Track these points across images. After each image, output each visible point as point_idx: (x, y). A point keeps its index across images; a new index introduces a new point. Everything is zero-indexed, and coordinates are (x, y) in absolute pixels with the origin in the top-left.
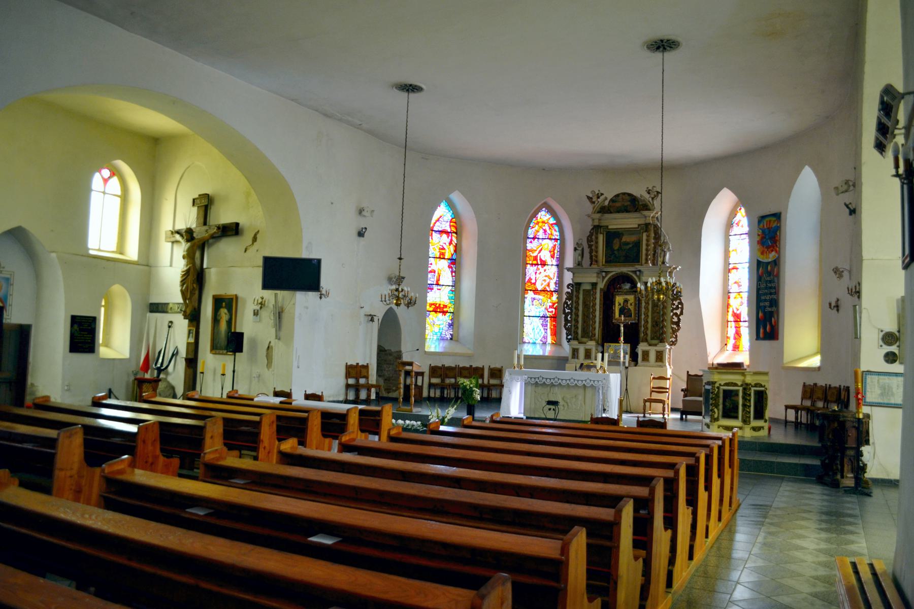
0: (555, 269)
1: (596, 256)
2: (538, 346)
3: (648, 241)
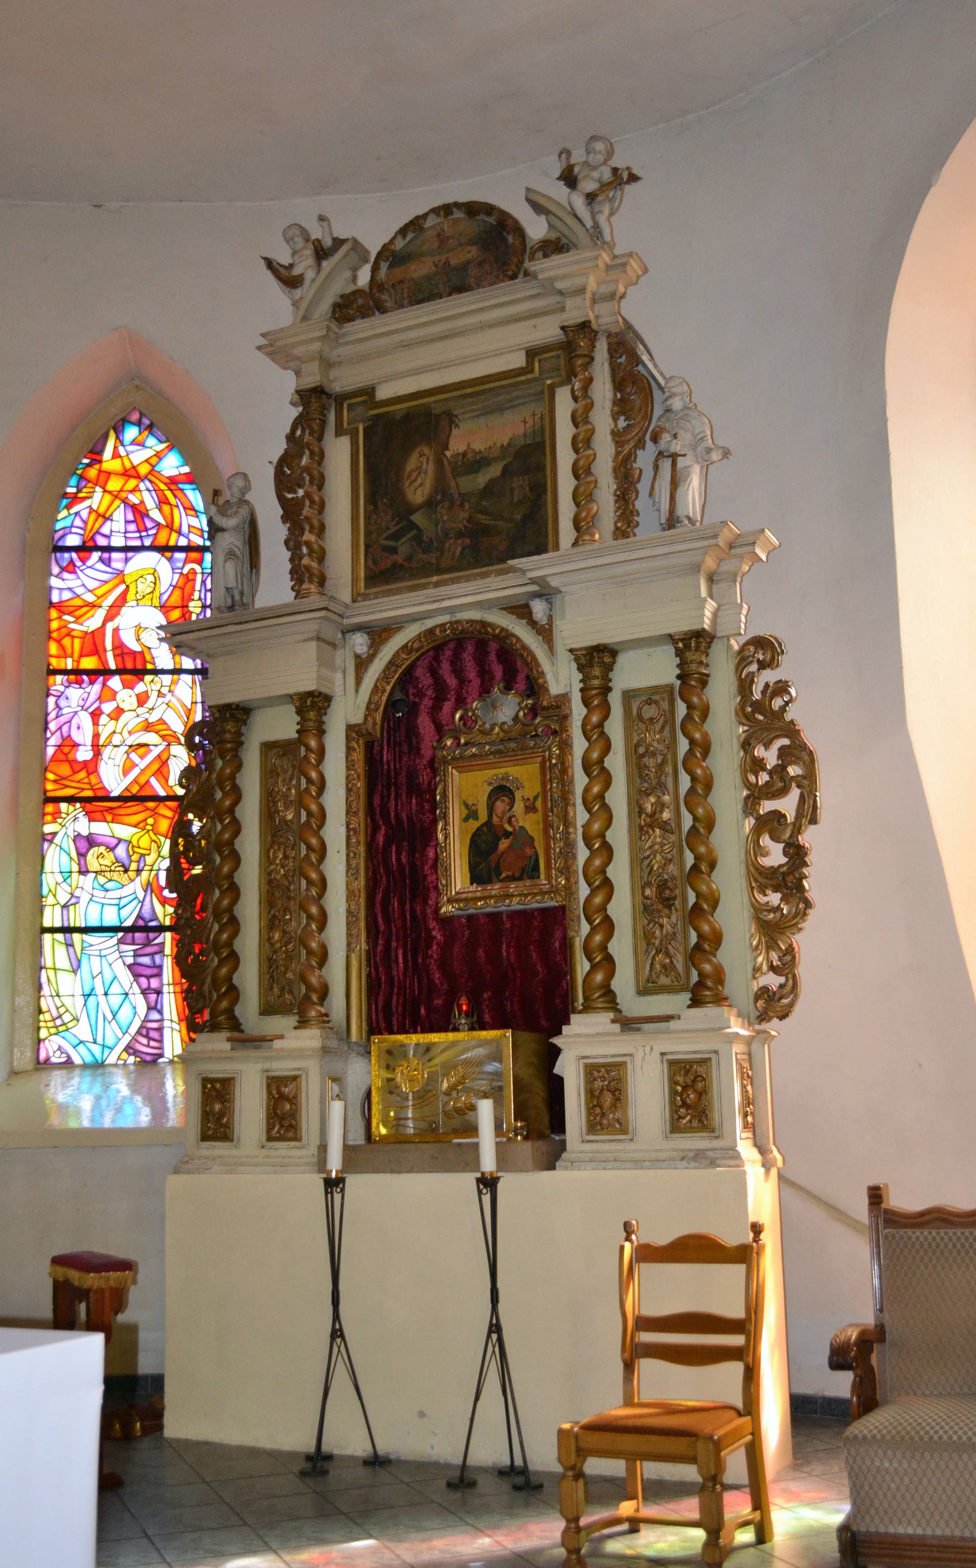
1: (321, 556)
2: (121, 1086)
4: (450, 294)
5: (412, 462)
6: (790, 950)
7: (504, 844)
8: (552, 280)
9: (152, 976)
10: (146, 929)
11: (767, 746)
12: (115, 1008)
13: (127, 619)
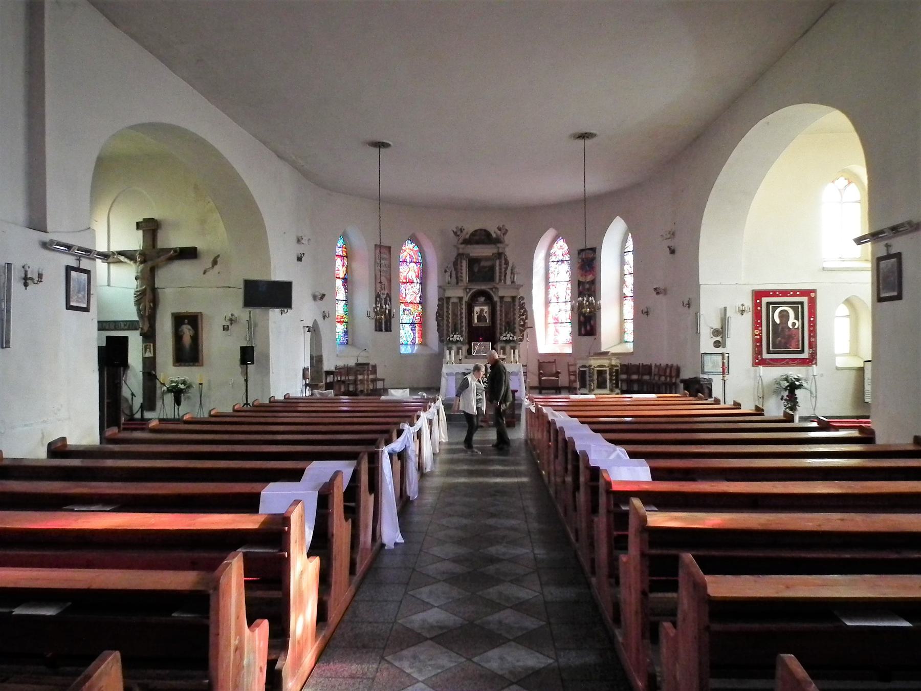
0: (418, 286)
3: (500, 265)
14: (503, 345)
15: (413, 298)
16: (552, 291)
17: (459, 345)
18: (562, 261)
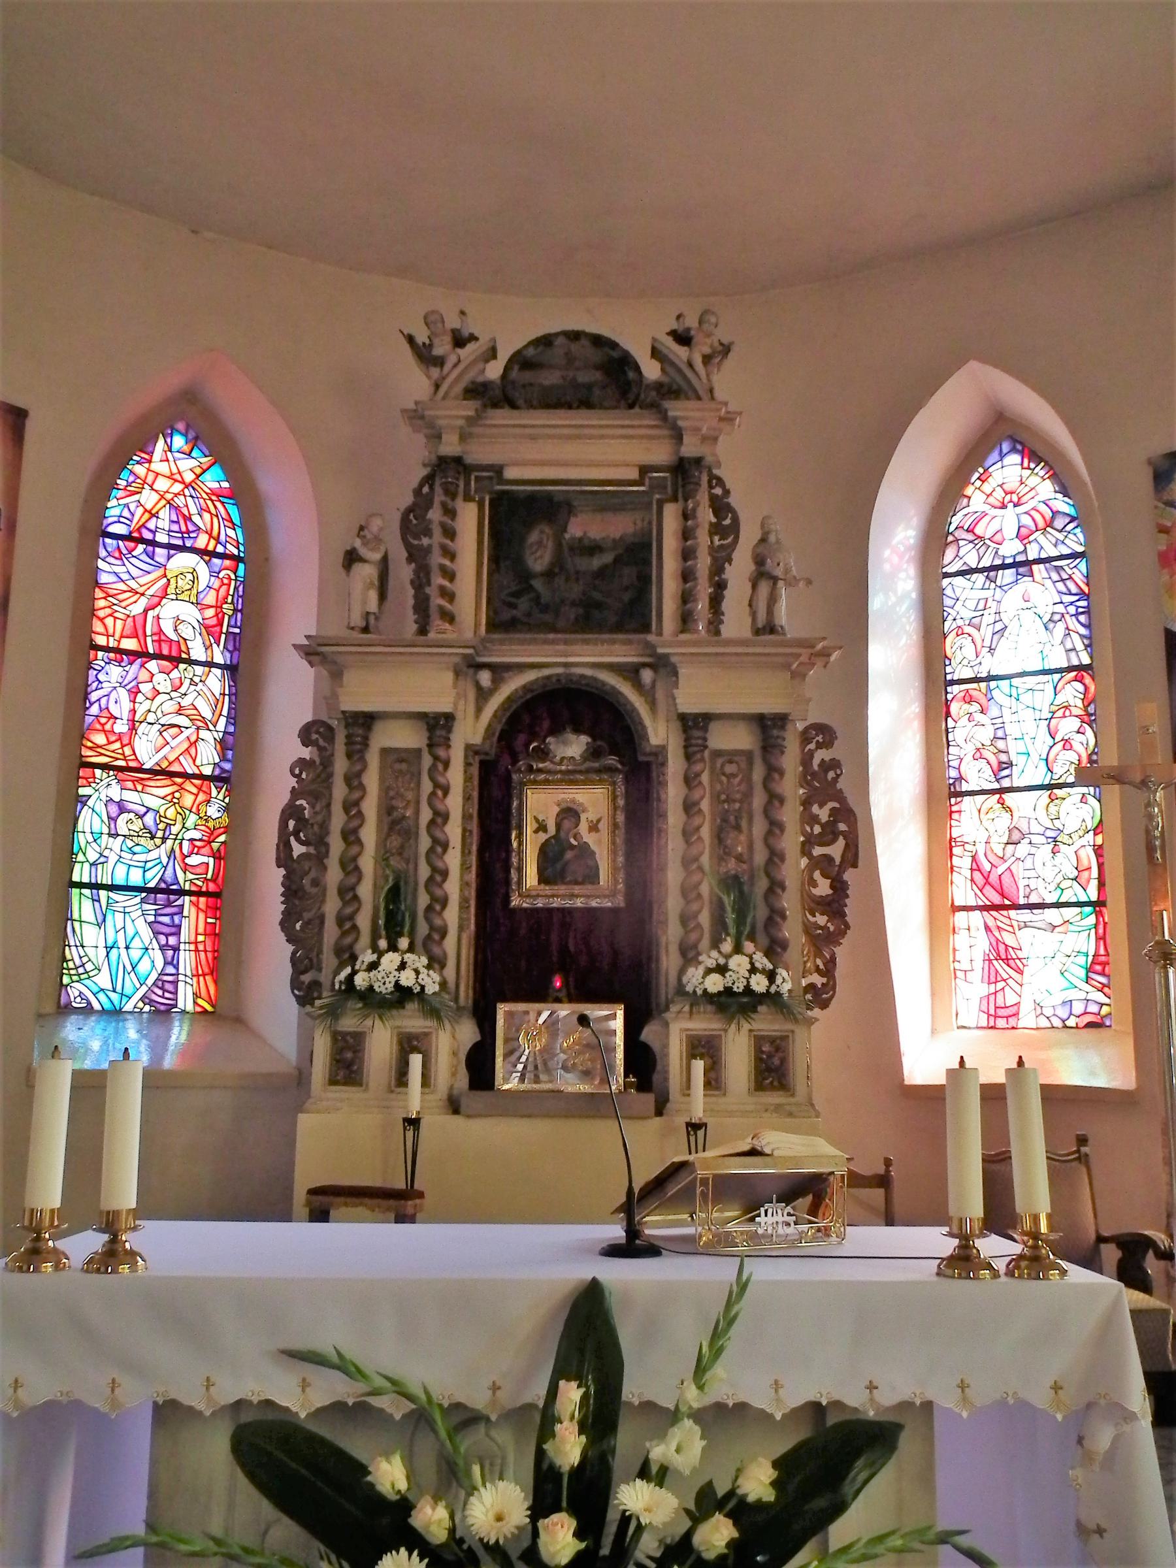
0: (215, 682)
3: (686, 534)
4: (578, 407)
5: (534, 537)
6: (833, 960)
7: (569, 855)
8: (676, 419)
9: (171, 934)
10: (167, 891)
11: (821, 806)
12: (135, 961)
13: (169, 610)
14: (704, 1023)
15: (179, 743)
16: (968, 732)
17: (412, 1020)
18: (1023, 566)
